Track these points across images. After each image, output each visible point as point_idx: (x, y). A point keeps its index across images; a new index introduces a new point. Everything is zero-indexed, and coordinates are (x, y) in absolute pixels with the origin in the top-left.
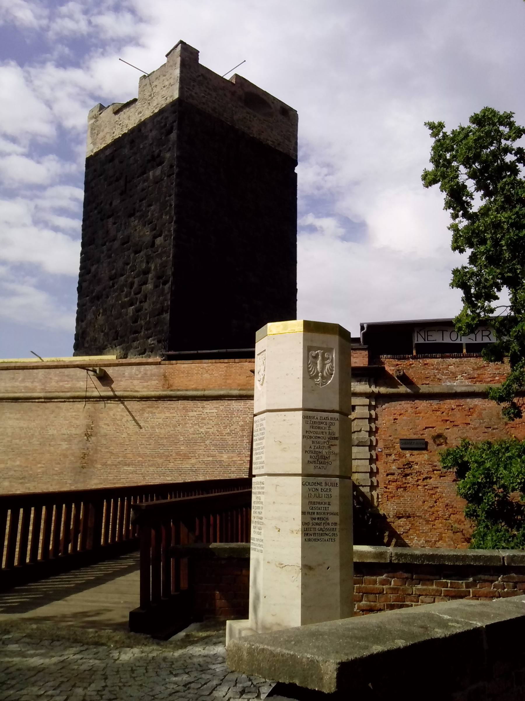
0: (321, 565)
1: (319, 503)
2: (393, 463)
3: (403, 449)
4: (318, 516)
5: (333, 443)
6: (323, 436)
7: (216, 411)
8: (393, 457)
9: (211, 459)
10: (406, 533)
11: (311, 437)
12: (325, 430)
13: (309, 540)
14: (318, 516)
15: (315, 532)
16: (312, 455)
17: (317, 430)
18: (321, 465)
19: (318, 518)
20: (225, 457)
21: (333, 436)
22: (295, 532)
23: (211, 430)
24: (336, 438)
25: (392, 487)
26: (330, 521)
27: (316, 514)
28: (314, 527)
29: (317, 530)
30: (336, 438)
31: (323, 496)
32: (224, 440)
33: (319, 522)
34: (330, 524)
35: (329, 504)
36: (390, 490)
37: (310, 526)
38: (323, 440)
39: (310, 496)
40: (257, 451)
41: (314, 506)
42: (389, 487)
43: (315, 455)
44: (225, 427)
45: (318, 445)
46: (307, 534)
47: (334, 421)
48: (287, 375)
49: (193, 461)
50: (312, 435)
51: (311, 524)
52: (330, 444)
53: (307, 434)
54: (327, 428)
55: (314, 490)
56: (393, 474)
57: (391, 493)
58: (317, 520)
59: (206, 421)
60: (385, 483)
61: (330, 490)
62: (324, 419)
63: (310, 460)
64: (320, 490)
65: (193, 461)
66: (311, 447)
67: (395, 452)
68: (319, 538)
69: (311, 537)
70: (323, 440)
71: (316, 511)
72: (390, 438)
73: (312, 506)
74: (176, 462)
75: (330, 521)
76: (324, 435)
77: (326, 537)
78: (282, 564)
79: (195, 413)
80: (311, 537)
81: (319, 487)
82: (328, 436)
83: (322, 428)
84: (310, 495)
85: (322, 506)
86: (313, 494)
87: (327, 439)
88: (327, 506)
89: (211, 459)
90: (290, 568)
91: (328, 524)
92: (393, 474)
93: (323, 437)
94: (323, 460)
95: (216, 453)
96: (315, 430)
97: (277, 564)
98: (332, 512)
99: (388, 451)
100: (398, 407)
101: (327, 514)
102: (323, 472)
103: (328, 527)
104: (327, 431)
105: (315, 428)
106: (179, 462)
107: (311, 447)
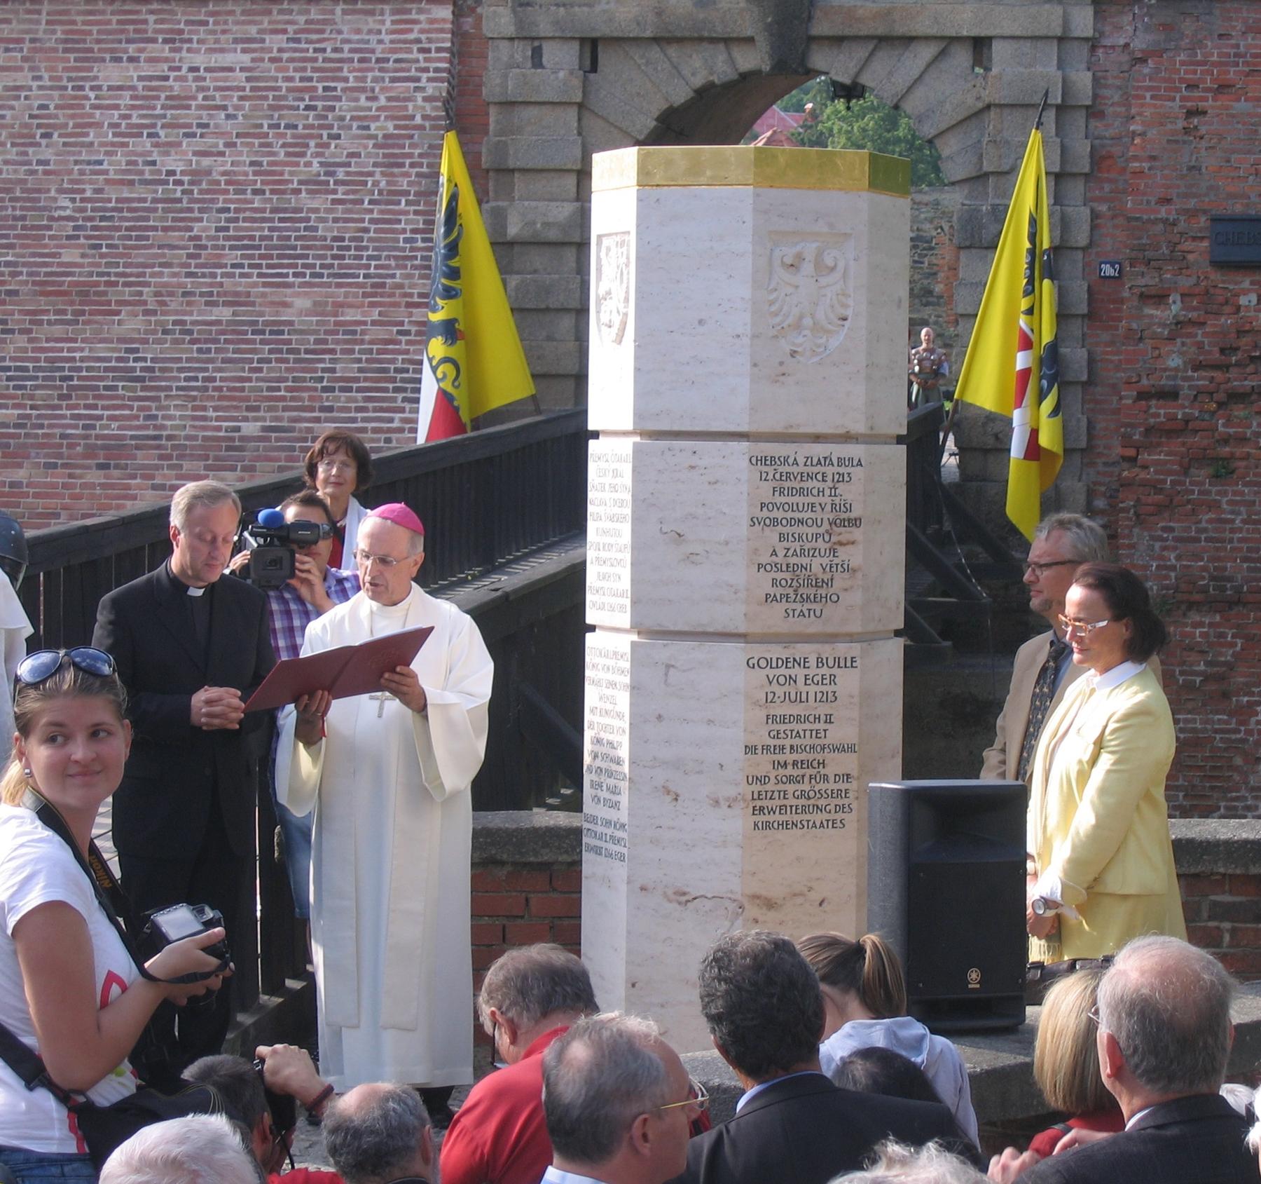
0: (801, 894)
1: (798, 719)
2: (1171, 338)
3: (1219, 265)
4: (795, 756)
5: (843, 538)
6: (813, 515)
7: (246, 59)
8: (1175, 307)
9: (225, 313)
10: (1221, 678)
11: (775, 522)
12: (821, 499)
13: (768, 825)
14: (795, 756)
15: (785, 802)
16: (779, 576)
17: (796, 499)
18: (807, 605)
19: (795, 763)
20: (302, 303)
21: (843, 516)
22: (724, 805)
23: (225, 164)
24: (856, 522)
25: (1160, 459)
26: (829, 771)
27: (787, 750)
28: (781, 787)
29: (790, 796)
30: (856, 522)
31: (811, 697)
32: (293, 216)
33: (796, 772)
34: (832, 779)
35: (829, 720)
36: (1151, 474)
37: (769, 787)
38: (814, 530)
39: (769, 700)
40: (603, 555)
41: (782, 727)
42: (1144, 457)
43: (788, 576)
44: (297, 150)
45: (797, 546)
46: (761, 809)
47: (849, 470)
48: (701, 322)
49: (131, 323)
50: (779, 514)
51: (773, 780)
52: (834, 539)
53: (765, 513)
54: (827, 492)
55: (782, 680)
56: (1171, 395)
57: (1155, 486)
58: (790, 767)
59: (191, 115)
60: (1127, 442)
61: (833, 679)
62: (819, 462)
63: (772, 591)
64: (801, 680)
65: (131, 323)
66: (774, 553)
67: (1186, 282)
68: (796, 818)
69: (771, 818)
70: (814, 530)
71: (788, 742)
72: (1163, 212)
73: (777, 727)
74: (40, 333)
75: (829, 771)
76: (818, 515)
77: (818, 817)
78: (684, 894)
79: (133, 73)
80: (771, 818)
81: (798, 672)
82: (828, 515)
83: (809, 492)
84: (770, 696)
85: (807, 726)
86: (780, 691)
87: (826, 526)
88: (822, 726)
89: (225, 313)
90: (709, 904)
91: (825, 778)
92: (1171, 395)
93: (815, 521)
94: (811, 591)
95: (250, 283)
96: (790, 500)
97: (670, 892)
98: (837, 743)
99: (1149, 280)
100: (1213, 51)
101: (823, 749)
102: (813, 626)
103: (822, 786)
104: (827, 500)
105: (791, 491)
106: (58, 330)
107: (774, 553)
